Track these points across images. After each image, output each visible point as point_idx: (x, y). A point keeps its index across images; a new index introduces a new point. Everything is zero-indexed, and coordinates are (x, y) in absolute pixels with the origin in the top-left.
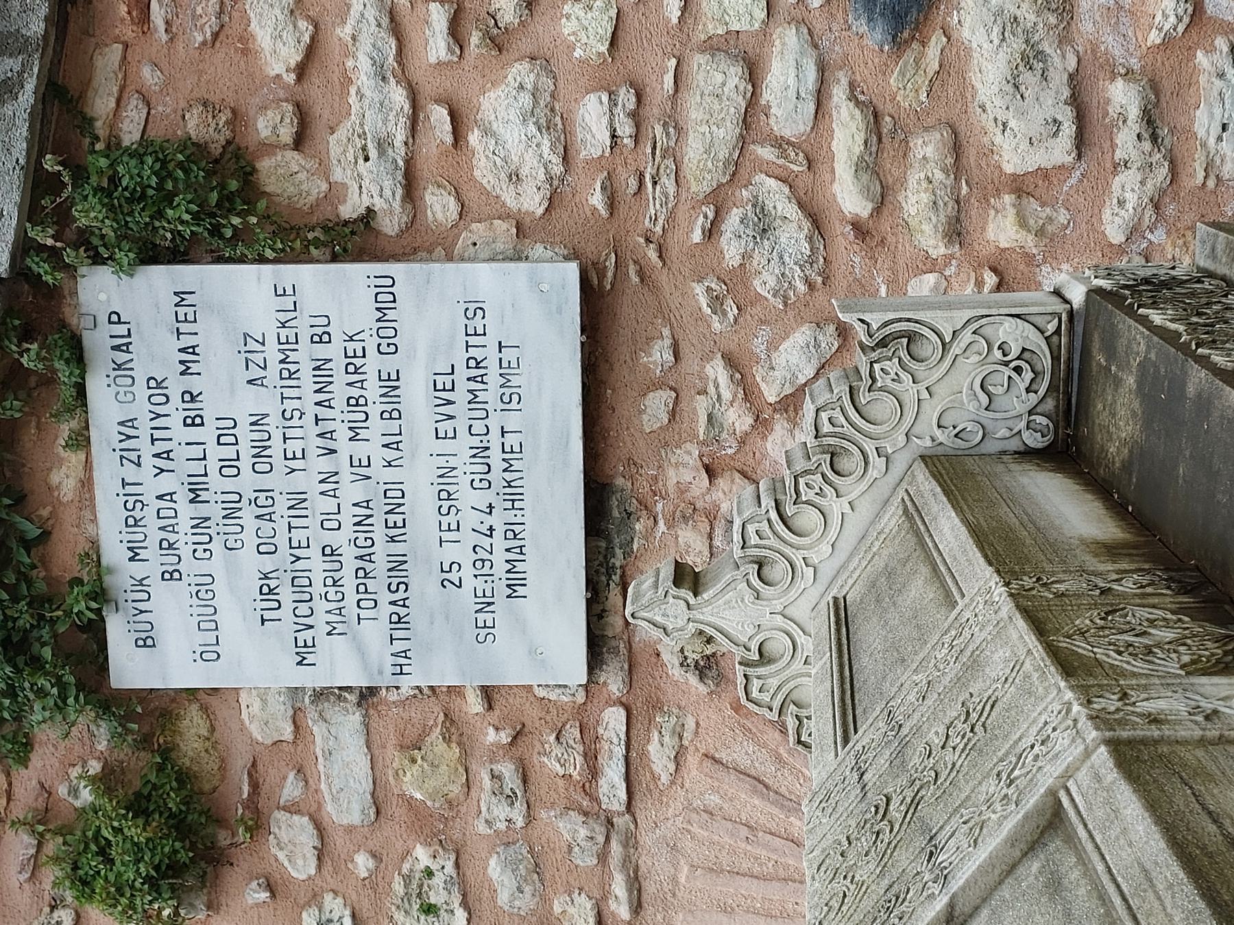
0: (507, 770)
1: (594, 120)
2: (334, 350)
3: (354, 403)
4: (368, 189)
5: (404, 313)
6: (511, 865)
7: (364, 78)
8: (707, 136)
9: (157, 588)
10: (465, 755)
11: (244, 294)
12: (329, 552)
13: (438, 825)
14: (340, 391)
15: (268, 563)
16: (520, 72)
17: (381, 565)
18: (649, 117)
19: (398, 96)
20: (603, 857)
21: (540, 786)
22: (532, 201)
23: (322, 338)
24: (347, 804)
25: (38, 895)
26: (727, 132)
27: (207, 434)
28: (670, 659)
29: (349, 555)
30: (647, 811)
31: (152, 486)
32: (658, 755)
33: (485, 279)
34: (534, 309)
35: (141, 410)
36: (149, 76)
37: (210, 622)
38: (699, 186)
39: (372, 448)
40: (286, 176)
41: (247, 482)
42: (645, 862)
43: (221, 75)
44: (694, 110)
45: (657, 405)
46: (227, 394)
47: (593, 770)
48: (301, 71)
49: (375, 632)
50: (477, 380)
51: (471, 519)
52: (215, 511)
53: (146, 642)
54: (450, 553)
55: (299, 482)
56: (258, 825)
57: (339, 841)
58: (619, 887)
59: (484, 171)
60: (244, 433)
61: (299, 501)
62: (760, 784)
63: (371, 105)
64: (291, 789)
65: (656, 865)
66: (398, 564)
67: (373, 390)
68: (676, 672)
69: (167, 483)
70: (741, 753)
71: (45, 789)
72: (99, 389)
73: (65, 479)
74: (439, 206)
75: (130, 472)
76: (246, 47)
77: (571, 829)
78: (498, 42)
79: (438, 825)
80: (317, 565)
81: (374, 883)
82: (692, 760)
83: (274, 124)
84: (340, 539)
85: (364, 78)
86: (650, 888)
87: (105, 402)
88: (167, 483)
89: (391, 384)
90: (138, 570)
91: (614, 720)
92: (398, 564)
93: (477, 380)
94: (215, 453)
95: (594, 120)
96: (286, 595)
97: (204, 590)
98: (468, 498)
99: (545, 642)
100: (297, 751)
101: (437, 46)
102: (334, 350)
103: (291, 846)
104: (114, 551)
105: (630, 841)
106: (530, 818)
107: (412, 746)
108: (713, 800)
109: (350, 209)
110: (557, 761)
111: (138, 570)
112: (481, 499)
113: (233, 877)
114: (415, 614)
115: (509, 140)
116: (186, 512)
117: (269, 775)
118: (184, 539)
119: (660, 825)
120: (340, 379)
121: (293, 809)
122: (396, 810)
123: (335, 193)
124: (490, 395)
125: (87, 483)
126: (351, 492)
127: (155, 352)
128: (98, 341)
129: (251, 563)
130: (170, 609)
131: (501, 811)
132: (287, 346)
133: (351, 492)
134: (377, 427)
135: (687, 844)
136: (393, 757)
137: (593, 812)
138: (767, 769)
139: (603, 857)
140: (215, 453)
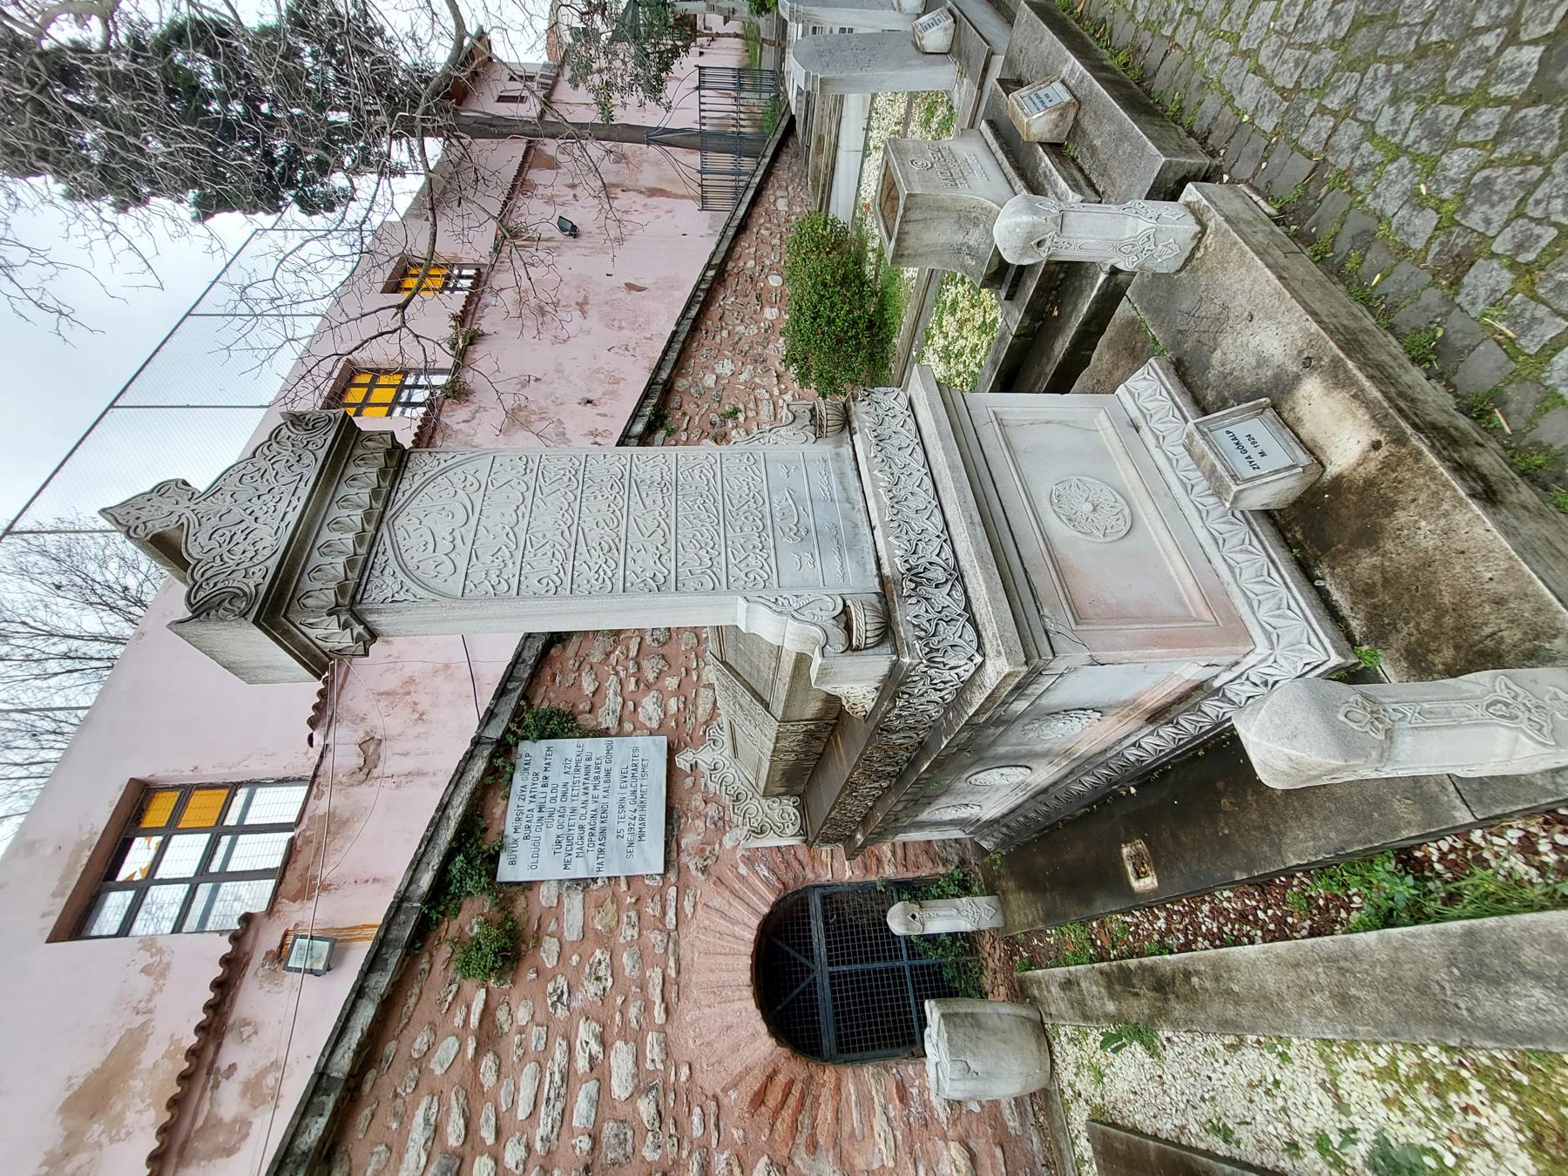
0: (633, 914)
1: (673, 705)
2: (592, 763)
3: (596, 778)
4: (609, 722)
5: (614, 752)
6: (631, 956)
7: (611, 695)
8: (703, 709)
9: (521, 843)
10: (618, 909)
11: (568, 747)
12: (581, 827)
13: (605, 939)
14: (592, 775)
15: (560, 832)
16: (653, 693)
17: (598, 830)
18: (688, 704)
19: (620, 699)
20: (666, 950)
21: (644, 922)
22: (655, 725)
23: (589, 759)
24: (572, 934)
25: (446, 978)
26: (709, 706)
27: (548, 789)
28: (692, 867)
29: (587, 827)
30: (683, 930)
31: (527, 806)
32: (688, 905)
33: (641, 741)
34: (653, 751)
35: (529, 783)
36: (552, 695)
37: (536, 855)
38: (702, 720)
39: (600, 793)
40: (586, 720)
41: (559, 804)
42: (682, 952)
43: (572, 695)
44: (700, 701)
45: (689, 781)
46: (557, 777)
47: (664, 914)
48: (594, 693)
49: (592, 856)
50: (636, 770)
51: (629, 814)
52: (546, 815)
53: (512, 863)
54: (621, 826)
55: (575, 804)
56: (538, 942)
57: (567, 947)
58: (672, 963)
59: (641, 718)
60: (560, 789)
61: (573, 810)
62: (723, 915)
63: (612, 701)
64: (553, 927)
65: (685, 952)
66: (603, 831)
67: (603, 774)
68: (694, 872)
69: (532, 806)
70: (717, 902)
71: (461, 929)
72: (517, 777)
73: (498, 811)
74: (628, 727)
75: (521, 803)
76: (580, 686)
77: (655, 937)
78: (649, 686)
79: (605, 939)
80: (576, 832)
81: (579, 968)
82: (699, 907)
83: (583, 706)
84: (585, 823)
85: (611, 695)
86: (683, 964)
87: (518, 779)
88: (532, 806)
89: (608, 773)
90: (516, 836)
91: (672, 891)
92: (603, 831)
93: (636, 770)
94: (550, 795)
95: (673, 705)
96: (564, 843)
97: (536, 844)
98: (629, 807)
99: (650, 858)
100: (557, 911)
101: (632, 687)
102: (592, 763)
103: (548, 954)
104: (509, 830)
105: (676, 944)
106: (640, 934)
107: (600, 906)
108: (707, 923)
109: (604, 726)
110: (651, 909)
111: (516, 836)
112: (632, 808)
113: (524, 966)
114: (607, 848)
115: (649, 708)
116: (536, 815)
117: (545, 922)
118: (533, 825)
119: (689, 934)
120: (593, 770)
121: (551, 935)
122: (590, 935)
123: (599, 724)
124: (638, 775)
125: (505, 812)
126: (591, 806)
127: (538, 765)
128: (520, 763)
129: (555, 831)
130: (523, 850)
131: (630, 932)
132: (578, 762)
133: (591, 806)
134: (602, 785)
135: (697, 943)
136: (592, 911)
137: (663, 930)
138: (726, 908)
139: (666, 950)
140: (550, 795)
